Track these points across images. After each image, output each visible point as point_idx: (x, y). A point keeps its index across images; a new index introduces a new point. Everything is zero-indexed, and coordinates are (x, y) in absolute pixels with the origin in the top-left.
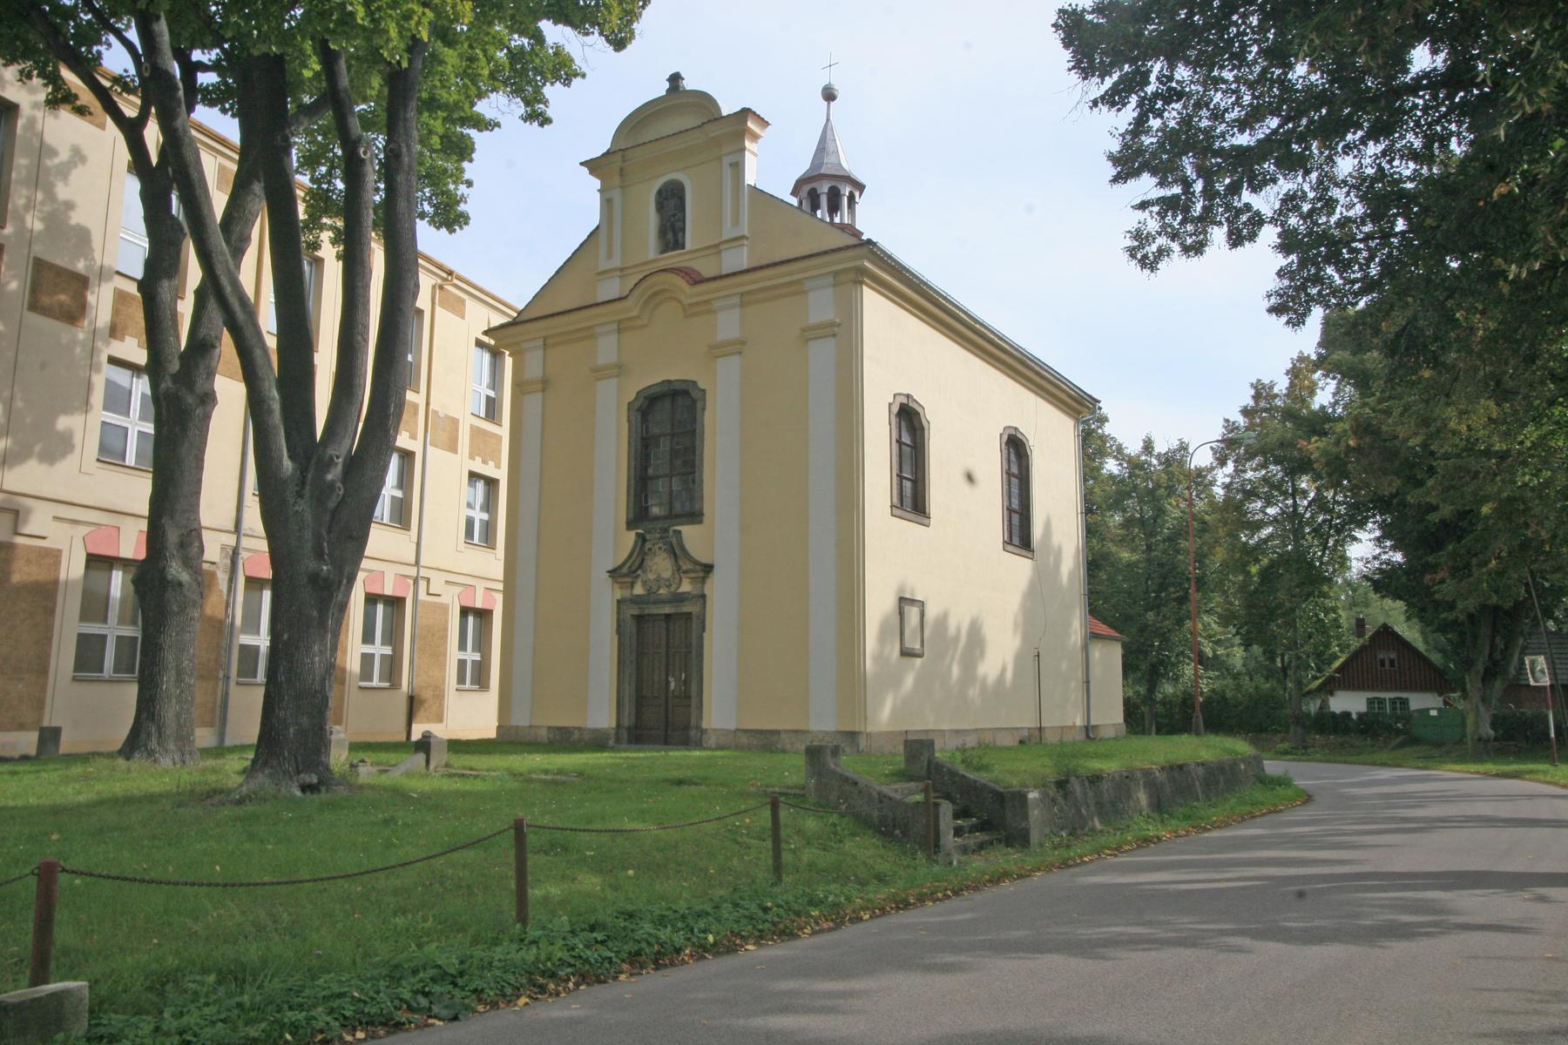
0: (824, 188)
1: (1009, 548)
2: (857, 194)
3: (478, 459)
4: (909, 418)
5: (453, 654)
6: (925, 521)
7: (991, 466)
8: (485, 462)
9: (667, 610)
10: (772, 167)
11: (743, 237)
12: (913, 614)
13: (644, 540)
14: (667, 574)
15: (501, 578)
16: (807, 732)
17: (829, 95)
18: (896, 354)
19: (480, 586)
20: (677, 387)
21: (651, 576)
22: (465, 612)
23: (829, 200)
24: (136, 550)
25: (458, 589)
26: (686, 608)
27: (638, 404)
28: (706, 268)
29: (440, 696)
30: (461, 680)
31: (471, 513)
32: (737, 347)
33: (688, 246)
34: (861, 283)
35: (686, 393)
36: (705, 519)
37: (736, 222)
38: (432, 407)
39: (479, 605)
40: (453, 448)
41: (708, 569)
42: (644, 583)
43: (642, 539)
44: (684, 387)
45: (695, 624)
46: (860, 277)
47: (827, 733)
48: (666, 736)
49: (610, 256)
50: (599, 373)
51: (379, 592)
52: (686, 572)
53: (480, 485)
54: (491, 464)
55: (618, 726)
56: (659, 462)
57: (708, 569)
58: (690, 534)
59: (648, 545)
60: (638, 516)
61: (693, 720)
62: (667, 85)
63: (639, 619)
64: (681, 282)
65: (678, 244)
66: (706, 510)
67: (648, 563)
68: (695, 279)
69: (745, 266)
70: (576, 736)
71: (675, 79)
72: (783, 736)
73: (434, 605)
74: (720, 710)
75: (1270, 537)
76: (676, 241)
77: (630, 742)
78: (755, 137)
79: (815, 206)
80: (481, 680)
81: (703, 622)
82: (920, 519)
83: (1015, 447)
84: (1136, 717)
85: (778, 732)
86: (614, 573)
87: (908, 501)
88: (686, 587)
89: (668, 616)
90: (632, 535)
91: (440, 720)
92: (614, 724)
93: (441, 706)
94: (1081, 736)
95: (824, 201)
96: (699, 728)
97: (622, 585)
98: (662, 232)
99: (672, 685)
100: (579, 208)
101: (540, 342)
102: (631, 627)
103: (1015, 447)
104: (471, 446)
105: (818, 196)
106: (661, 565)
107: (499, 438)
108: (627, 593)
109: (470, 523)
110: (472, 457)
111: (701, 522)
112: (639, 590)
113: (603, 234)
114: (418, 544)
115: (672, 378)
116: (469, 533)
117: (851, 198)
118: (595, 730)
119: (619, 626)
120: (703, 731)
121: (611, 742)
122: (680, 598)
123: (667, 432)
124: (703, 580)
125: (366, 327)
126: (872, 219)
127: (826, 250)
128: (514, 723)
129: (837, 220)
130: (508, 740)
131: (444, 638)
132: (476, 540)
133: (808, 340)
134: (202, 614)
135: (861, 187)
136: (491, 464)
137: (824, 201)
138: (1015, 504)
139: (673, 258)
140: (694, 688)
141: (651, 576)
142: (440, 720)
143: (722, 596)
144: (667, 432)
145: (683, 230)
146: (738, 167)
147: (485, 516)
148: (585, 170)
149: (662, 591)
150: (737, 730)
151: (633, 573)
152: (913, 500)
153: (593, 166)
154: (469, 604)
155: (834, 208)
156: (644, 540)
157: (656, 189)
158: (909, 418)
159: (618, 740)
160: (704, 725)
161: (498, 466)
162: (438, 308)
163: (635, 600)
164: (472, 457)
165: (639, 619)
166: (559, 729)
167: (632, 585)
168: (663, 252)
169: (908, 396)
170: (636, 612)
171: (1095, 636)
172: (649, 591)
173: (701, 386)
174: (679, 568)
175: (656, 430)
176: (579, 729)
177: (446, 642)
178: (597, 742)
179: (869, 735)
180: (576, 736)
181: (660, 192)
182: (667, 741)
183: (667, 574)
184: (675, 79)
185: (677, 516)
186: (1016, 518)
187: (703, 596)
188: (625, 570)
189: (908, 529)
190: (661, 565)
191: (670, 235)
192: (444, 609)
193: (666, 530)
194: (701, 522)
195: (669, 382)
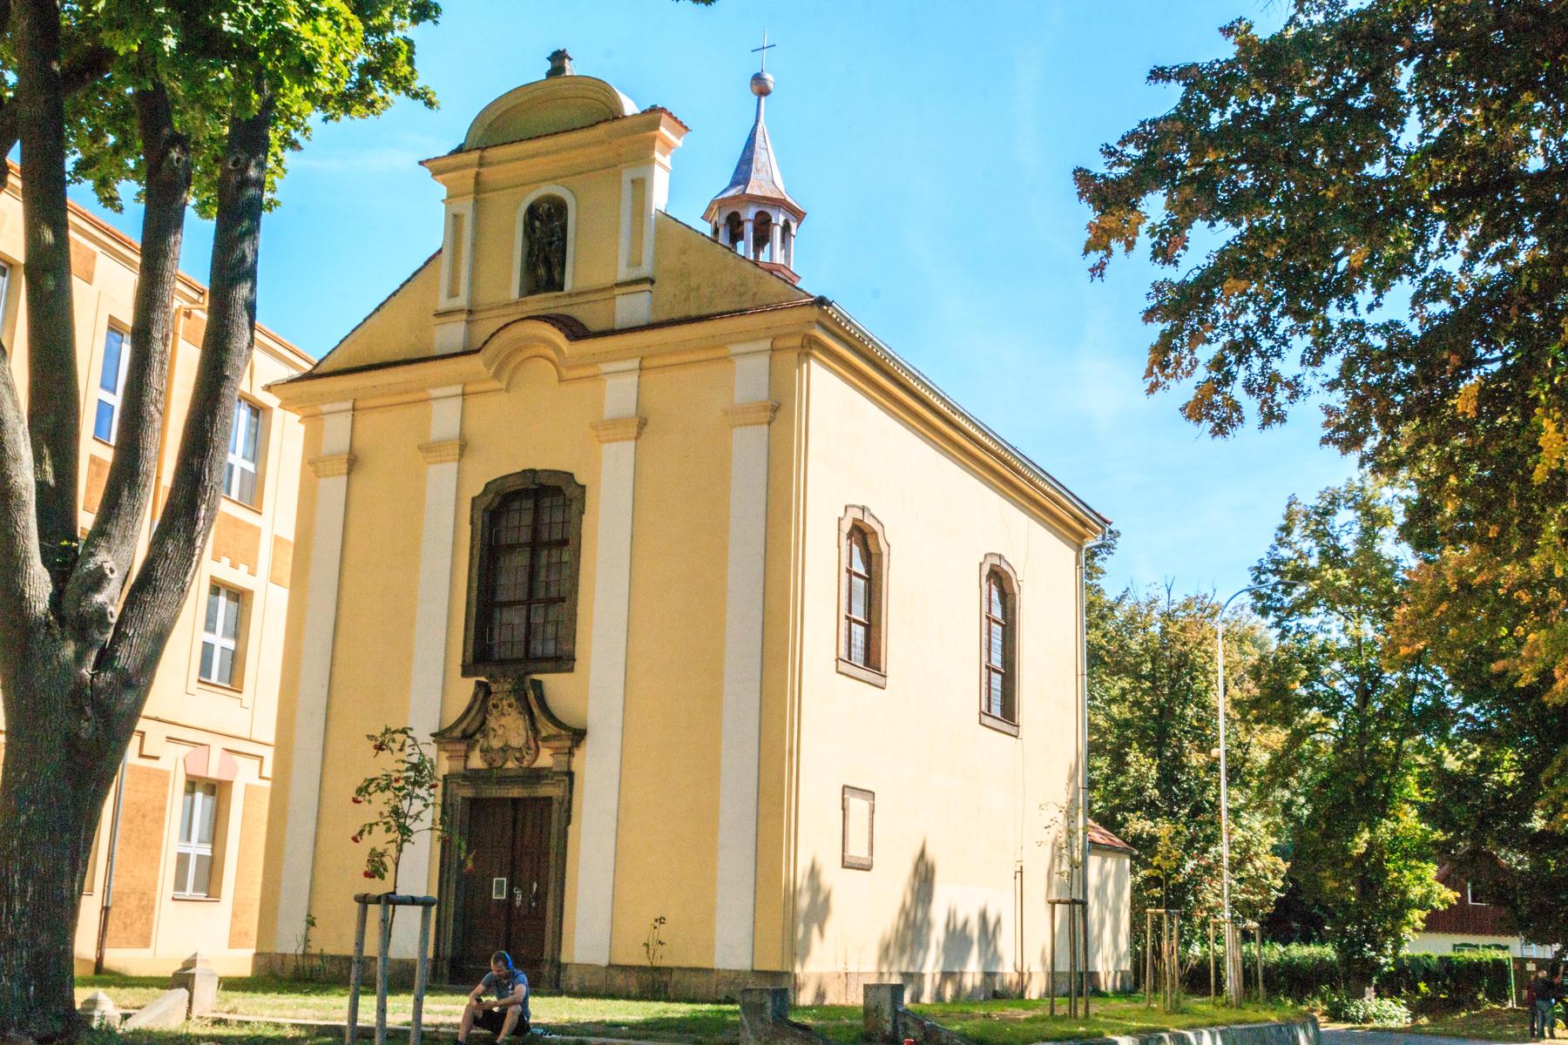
0: (749, 214)
2: (793, 225)
3: (226, 561)
5: (172, 844)
7: (968, 601)
8: (234, 565)
9: (516, 792)
10: (680, 187)
12: (858, 805)
13: (488, 693)
14: (517, 741)
15: (271, 739)
17: (760, 87)
18: (849, 447)
21: (496, 743)
22: (192, 785)
23: (755, 230)
25: (184, 750)
26: (544, 791)
28: (590, 315)
29: (147, 907)
30: (180, 884)
33: (568, 287)
34: (808, 355)
35: (558, 491)
36: (577, 666)
39: (213, 773)
43: (484, 691)
46: (809, 346)
49: (453, 294)
50: (430, 449)
51: (202, 773)
52: (545, 739)
56: (512, 580)
57: (579, 735)
58: (555, 684)
60: (482, 654)
62: (548, 66)
64: (557, 336)
65: (553, 283)
66: (577, 656)
67: (492, 722)
71: (558, 59)
73: (147, 772)
79: (736, 236)
80: (209, 878)
81: (569, 810)
83: (999, 579)
88: (545, 759)
90: (470, 684)
91: (145, 942)
93: (149, 922)
95: (749, 229)
98: (530, 265)
99: (519, 898)
100: (418, 222)
103: (999, 579)
105: (741, 224)
106: (509, 728)
107: (256, 532)
109: (207, 649)
111: (571, 670)
112: (476, 761)
113: (446, 256)
115: (539, 466)
116: (205, 669)
117: (786, 228)
118: (401, 962)
123: (524, 539)
125: (166, 393)
126: (811, 262)
127: (742, 290)
128: (280, 950)
129: (764, 257)
130: (275, 975)
131: (159, 821)
132: (214, 679)
133: (733, 426)
135: (799, 215)
136: (243, 568)
137: (749, 229)
138: (997, 662)
142: (145, 942)
143: (598, 778)
144: (524, 539)
146: (641, 186)
147: (230, 644)
148: (426, 172)
151: (468, 737)
153: (436, 167)
154: (198, 771)
155: (762, 239)
157: (525, 205)
160: (564, 959)
161: (252, 573)
163: (471, 776)
165: (474, 804)
169: (863, 509)
171: (1095, 847)
173: (580, 480)
174: (536, 731)
175: (507, 538)
177: (161, 827)
178: (400, 980)
184: (558, 59)
185: (537, 659)
186: (997, 680)
188: (457, 733)
189: (857, 692)
191: (542, 271)
192: (163, 777)
194: (571, 670)
195: (533, 471)
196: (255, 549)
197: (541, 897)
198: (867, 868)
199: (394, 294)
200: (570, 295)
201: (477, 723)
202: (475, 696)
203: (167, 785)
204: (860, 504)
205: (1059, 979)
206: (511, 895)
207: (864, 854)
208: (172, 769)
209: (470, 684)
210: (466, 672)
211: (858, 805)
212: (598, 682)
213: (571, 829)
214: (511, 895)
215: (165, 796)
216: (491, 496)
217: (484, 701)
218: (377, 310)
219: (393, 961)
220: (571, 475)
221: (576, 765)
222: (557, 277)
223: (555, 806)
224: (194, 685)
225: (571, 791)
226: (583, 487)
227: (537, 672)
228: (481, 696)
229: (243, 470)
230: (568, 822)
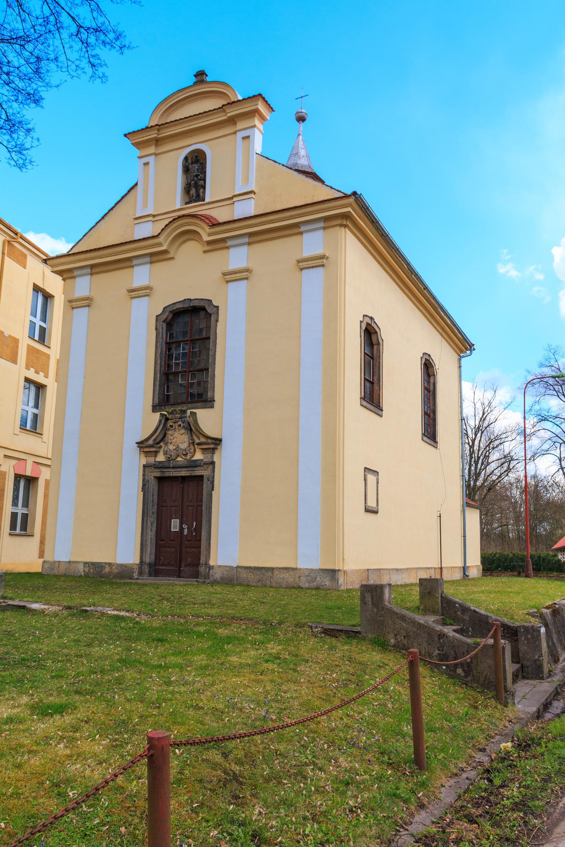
1: (425, 438)
3: (32, 370)
4: (370, 335)
6: (380, 413)
8: (37, 372)
11: (252, 192)
14: (184, 446)
16: (296, 569)
19: (30, 461)
20: (196, 304)
22: (18, 477)
25: (14, 462)
26: (198, 472)
27: (165, 316)
28: (221, 214)
31: (26, 408)
32: (242, 275)
33: (207, 200)
35: (203, 309)
36: (216, 404)
37: (246, 180)
39: (28, 473)
40: (14, 360)
41: (218, 442)
42: (165, 453)
44: (202, 304)
45: (206, 485)
47: (312, 570)
48: (180, 571)
53: (33, 389)
54: (42, 374)
55: (142, 561)
57: (218, 442)
59: (170, 423)
60: (162, 401)
61: (202, 560)
63: (160, 480)
67: (169, 437)
68: (214, 224)
69: (253, 214)
70: (107, 569)
72: (276, 572)
74: (227, 549)
75: (26, 597)
76: (198, 195)
77: (150, 575)
78: (263, 118)
81: (212, 483)
82: (376, 410)
83: (428, 367)
84: (492, 565)
85: (272, 569)
86: (141, 444)
87: (368, 396)
88: (199, 456)
89: (184, 478)
90: (157, 416)
92: (138, 561)
94: (458, 576)
96: (207, 564)
97: (147, 454)
98: (187, 189)
102: (153, 485)
103: (428, 367)
104: (27, 359)
106: (179, 439)
107: (48, 356)
108: (151, 460)
110: (28, 368)
111: (212, 407)
112: (161, 458)
118: (122, 565)
119: (144, 485)
120: (211, 568)
121: (135, 575)
122: (195, 464)
123: (187, 337)
124: (213, 450)
128: (57, 559)
136: (42, 374)
139: (195, 208)
140: (204, 534)
141: (171, 447)
144: (187, 337)
145: (204, 187)
149: (179, 459)
150: (237, 567)
151: (157, 443)
152: (372, 397)
156: (167, 419)
158: (370, 335)
159: (141, 573)
161: (46, 376)
162: (6, 258)
164: (28, 368)
165: (160, 480)
166: (93, 564)
167: (156, 453)
168: (186, 203)
169: (371, 318)
170: (158, 474)
172: (169, 460)
176: (110, 564)
179: (345, 572)
180: (107, 569)
181: (186, 159)
183: (184, 446)
187: (213, 463)
190: (179, 439)
191: (193, 191)
193: (184, 412)
194: (212, 407)
195: (190, 300)
196: (48, 365)
197: (198, 529)
198: (376, 512)
199: (112, 209)
200: (209, 203)
201: (161, 437)
202: (160, 421)
203: (5, 479)
204: (370, 316)
205: (75, 565)
206: (182, 529)
207: (374, 505)
208: (8, 471)
209: (157, 416)
210: (155, 408)
211: (371, 478)
212: (226, 416)
213: (213, 493)
214: (182, 529)
215: (4, 484)
216: (167, 314)
217: (165, 424)
218: (103, 218)
219: (480, 575)
220: (210, 301)
221: (216, 459)
222: (201, 194)
223: (205, 480)
224: (18, 430)
225: (214, 472)
226: (217, 307)
227: (193, 408)
228: (163, 421)
229: (40, 326)
230: (213, 490)
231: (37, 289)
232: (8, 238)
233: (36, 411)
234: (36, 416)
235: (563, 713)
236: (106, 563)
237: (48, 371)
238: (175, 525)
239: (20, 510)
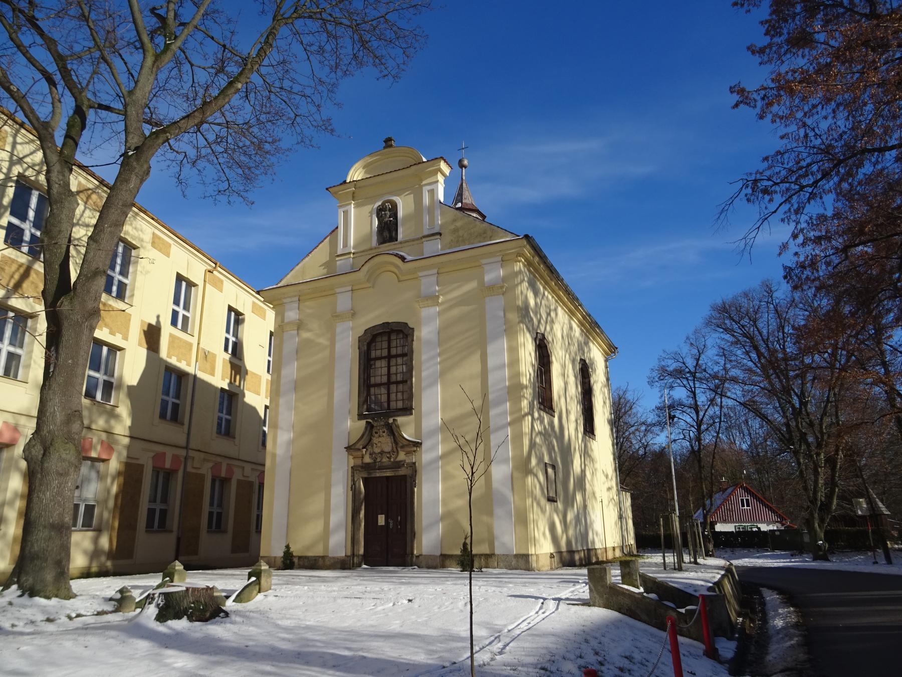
9: (388, 474)
21: (377, 450)
24: (127, 233)
31: (166, 398)
33: (400, 237)
38: (201, 346)
39: (223, 475)
50: (337, 317)
54: (119, 336)
61: (408, 549)
65: (393, 238)
101: (297, 299)
106: (383, 443)
108: (359, 462)
111: (411, 414)
112: (367, 459)
114: (188, 434)
118: (334, 558)
134: (18, 469)
162: (207, 284)
163: (366, 467)
179: (537, 556)
182: (142, 472)
190: (383, 443)
202: (366, 428)
224: (215, 434)
231: (231, 309)
232: (209, 268)
233: (228, 417)
234: (228, 421)
235: (9, 3)
236: (319, 557)
237: (128, 331)
238: (381, 520)
239: (216, 510)
